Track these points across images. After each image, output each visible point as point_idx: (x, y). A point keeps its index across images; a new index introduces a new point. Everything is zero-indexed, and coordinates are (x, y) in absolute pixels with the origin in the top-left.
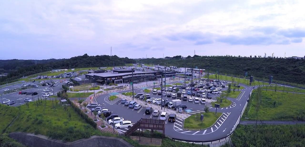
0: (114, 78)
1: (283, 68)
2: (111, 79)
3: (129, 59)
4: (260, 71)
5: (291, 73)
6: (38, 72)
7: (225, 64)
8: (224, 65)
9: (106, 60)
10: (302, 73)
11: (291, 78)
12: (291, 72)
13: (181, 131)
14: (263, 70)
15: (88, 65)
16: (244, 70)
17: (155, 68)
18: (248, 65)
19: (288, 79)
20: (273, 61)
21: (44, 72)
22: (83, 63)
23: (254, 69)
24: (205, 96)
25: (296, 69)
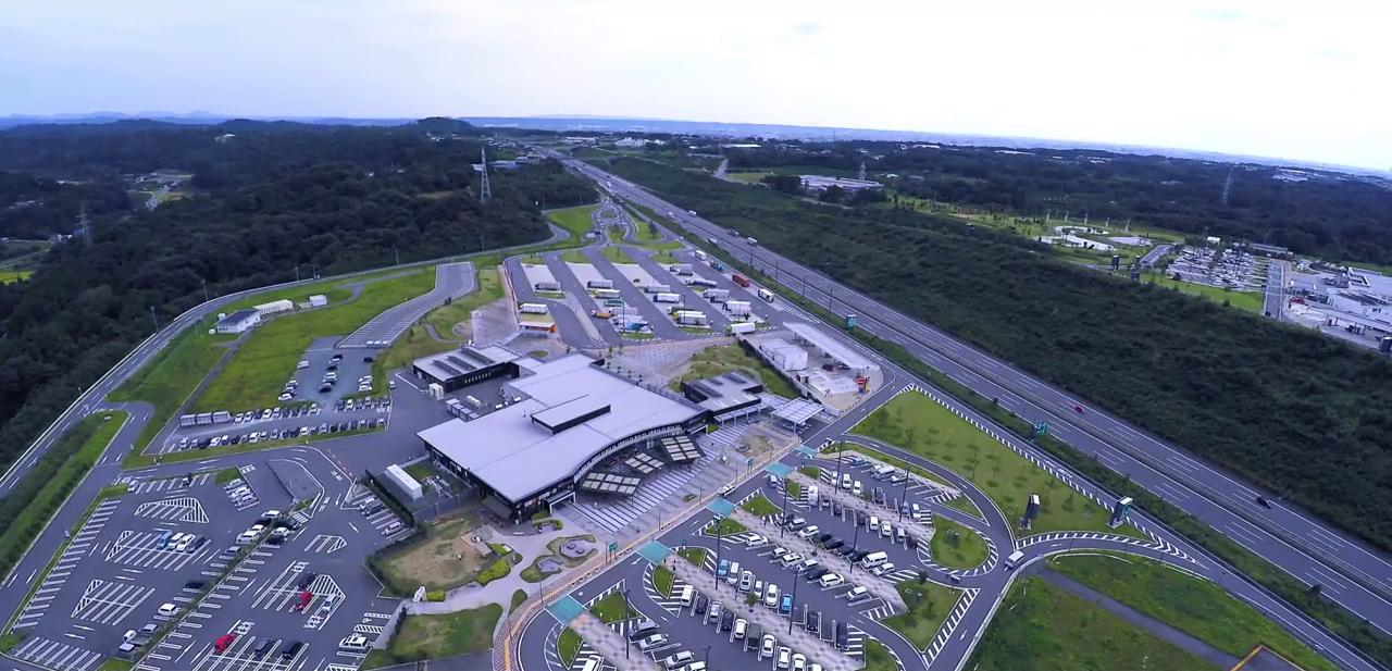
0: (548, 494)
1: (1246, 384)
2: (537, 501)
3: (592, 266)
4: (1129, 369)
5: (1276, 421)
6: (138, 333)
7: (985, 286)
8: (980, 291)
9: (464, 216)
10: (1331, 441)
11: (1264, 448)
12: (1277, 416)
13: (652, 594)
14: (1147, 365)
15: (384, 250)
16: (1060, 344)
17: (640, 215)
18: (1085, 319)
19: (1249, 452)
20: (1213, 325)
21: (170, 320)
22: (355, 242)
23: (1106, 347)
24: (859, 492)
25: (1307, 409)
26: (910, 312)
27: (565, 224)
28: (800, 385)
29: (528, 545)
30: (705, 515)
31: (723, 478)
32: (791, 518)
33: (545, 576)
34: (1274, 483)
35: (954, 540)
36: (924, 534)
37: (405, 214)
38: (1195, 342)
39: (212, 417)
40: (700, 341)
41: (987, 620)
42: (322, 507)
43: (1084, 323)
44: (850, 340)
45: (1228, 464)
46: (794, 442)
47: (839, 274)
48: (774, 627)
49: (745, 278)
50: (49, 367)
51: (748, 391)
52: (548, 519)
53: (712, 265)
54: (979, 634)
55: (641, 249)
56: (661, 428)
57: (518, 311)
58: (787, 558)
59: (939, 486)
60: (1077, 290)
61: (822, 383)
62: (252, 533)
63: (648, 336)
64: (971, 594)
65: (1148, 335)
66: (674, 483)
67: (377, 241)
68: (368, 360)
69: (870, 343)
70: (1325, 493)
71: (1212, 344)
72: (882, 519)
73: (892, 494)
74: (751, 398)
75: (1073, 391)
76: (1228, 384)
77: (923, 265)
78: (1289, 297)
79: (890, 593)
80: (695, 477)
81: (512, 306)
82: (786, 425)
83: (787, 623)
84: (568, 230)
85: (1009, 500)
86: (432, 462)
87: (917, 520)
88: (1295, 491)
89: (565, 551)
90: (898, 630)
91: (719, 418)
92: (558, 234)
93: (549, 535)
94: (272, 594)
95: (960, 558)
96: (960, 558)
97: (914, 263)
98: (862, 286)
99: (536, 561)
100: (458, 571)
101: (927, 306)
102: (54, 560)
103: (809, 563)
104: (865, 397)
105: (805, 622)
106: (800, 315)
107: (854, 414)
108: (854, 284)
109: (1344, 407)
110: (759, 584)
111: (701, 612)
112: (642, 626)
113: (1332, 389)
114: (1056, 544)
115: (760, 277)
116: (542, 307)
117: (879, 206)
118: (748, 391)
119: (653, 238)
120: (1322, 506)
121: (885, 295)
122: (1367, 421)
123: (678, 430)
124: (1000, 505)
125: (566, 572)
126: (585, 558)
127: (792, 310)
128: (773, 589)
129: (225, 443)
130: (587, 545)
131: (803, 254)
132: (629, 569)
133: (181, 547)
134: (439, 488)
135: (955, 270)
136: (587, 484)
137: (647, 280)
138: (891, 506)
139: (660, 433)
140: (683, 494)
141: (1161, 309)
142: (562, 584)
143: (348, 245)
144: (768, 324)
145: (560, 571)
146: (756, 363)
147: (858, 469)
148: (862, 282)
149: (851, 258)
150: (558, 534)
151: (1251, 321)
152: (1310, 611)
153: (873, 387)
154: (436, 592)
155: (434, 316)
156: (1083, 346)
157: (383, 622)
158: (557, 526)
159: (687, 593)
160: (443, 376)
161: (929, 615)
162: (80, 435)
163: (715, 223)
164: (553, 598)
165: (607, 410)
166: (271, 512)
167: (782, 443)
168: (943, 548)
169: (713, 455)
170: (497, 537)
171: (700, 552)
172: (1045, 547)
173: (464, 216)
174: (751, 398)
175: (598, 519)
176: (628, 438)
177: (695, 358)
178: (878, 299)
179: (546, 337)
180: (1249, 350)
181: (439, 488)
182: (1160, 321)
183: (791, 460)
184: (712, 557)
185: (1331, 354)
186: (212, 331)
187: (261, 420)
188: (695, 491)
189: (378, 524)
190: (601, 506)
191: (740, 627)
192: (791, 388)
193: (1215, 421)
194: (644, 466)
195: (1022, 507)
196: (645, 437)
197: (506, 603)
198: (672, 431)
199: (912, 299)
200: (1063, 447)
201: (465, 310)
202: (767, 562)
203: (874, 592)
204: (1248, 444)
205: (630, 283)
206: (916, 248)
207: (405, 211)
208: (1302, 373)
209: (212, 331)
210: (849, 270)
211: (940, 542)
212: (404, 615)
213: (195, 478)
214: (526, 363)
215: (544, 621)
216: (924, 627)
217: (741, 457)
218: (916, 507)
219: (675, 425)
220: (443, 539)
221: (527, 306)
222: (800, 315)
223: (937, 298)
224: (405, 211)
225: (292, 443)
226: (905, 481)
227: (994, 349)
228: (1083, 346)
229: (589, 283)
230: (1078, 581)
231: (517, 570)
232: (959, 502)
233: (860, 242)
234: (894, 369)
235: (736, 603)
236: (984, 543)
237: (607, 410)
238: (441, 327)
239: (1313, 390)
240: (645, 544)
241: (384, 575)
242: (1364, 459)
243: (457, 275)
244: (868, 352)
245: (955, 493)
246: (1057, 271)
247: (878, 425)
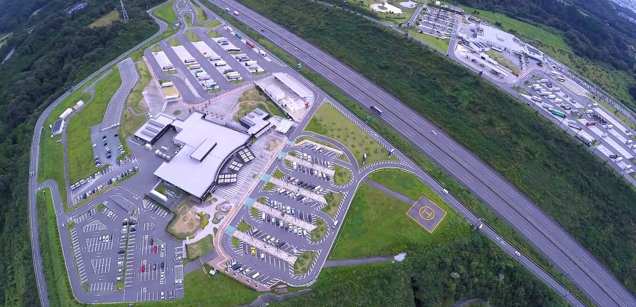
3: (182, 46)
11: (439, 112)
19: (435, 114)
22: (80, 65)
27: (163, 18)
29: (209, 210)
30: (262, 182)
31: (262, 163)
32: (289, 178)
33: (220, 220)
34: (440, 125)
35: (340, 175)
36: (331, 173)
37: (94, 39)
38: (423, 67)
39: (80, 183)
40: (239, 89)
41: (350, 202)
42: (139, 212)
43: (388, 57)
44: (300, 76)
45: (429, 118)
47: (289, 26)
48: (289, 219)
50: (9, 174)
52: (211, 198)
53: (236, 35)
54: (348, 208)
55: (202, 28)
56: (237, 149)
57: (160, 86)
58: (290, 195)
59: (335, 150)
60: (386, 40)
62: (125, 230)
64: (346, 193)
65: (409, 63)
66: (247, 171)
67: (90, 60)
68: (116, 136)
70: (454, 129)
71: (429, 68)
72: (319, 170)
73: (319, 157)
75: (383, 87)
76: (432, 86)
77: (327, 24)
78: (458, 40)
79: (322, 200)
80: (254, 166)
81: (158, 84)
83: (294, 218)
84: (167, 22)
85: (358, 152)
86: (164, 185)
87: (329, 168)
88: (446, 128)
89: (223, 210)
90: (325, 212)
91: (257, 136)
92: (163, 26)
93: (215, 204)
94: (144, 251)
95: (342, 181)
96: (342, 181)
98: (302, 35)
99: (215, 216)
100: (193, 226)
101: (329, 46)
102: (75, 257)
103: (297, 195)
104: (309, 108)
105: (299, 216)
110: (284, 207)
111: (269, 221)
112: (254, 231)
113: (463, 89)
114: (371, 168)
116: (170, 83)
119: (206, 19)
120: (453, 134)
121: (312, 40)
122: (470, 102)
123: (244, 147)
124: (355, 155)
125: (225, 217)
126: (229, 211)
127: (277, 61)
128: (288, 208)
129: (91, 194)
130: (227, 205)
131: (274, 17)
132: (243, 211)
133: (107, 241)
134: (172, 195)
135: (339, 28)
136: (220, 181)
137: (210, 53)
138: (321, 164)
139: (237, 150)
140: (252, 175)
141: (414, 51)
142: (226, 222)
143: (79, 67)
145: (223, 217)
146: (264, 98)
147: (309, 149)
148: (302, 33)
150: (217, 203)
152: (438, 180)
154: (191, 235)
155: (129, 101)
156: (387, 68)
157: (181, 249)
158: (216, 200)
159: (264, 217)
160: (149, 139)
161: (334, 205)
162: (42, 204)
164: (225, 228)
165: (216, 144)
166: (125, 220)
167: (281, 141)
168: (338, 178)
169: (257, 154)
170: (199, 210)
171: (263, 199)
172: (367, 171)
173: (120, 33)
174: (266, 123)
175: (227, 193)
177: (240, 100)
178: (309, 42)
180: (440, 72)
181: (172, 195)
182: (413, 57)
184: (267, 199)
186: (52, 136)
187: (96, 179)
188: (256, 173)
189: (160, 214)
190: (227, 187)
191: (281, 224)
193: (426, 101)
194: (236, 168)
196: (233, 153)
197: (212, 233)
198: (241, 148)
199: (323, 42)
201: (140, 92)
202: (284, 197)
203: (318, 200)
204: (435, 111)
205: (201, 54)
207: (94, 37)
208: (455, 82)
209: (52, 136)
211: (336, 176)
212: (186, 246)
213: (91, 211)
214: (176, 124)
215: (225, 236)
216: (333, 209)
217: (268, 152)
218: (329, 163)
219: (242, 146)
220: (183, 215)
221: (164, 84)
223: (333, 42)
224: (94, 37)
225: (112, 187)
226: (325, 151)
227: (356, 68)
228: (387, 68)
229: (185, 61)
230: (376, 182)
231: (210, 220)
232: (342, 157)
233: (299, 10)
235: (278, 214)
236: (350, 172)
237: (216, 144)
238: (134, 106)
240: (245, 199)
241: (174, 234)
242: (467, 116)
243: (125, 65)
244: (308, 81)
245: (341, 153)
246: (379, 31)
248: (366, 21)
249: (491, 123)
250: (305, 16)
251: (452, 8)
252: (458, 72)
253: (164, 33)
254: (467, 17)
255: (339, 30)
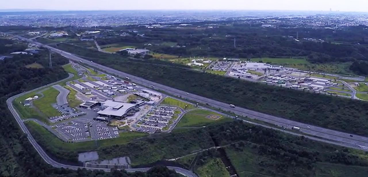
26: (164, 84)
28: (149, 99)
46: (152, 106)
49: (120, 79)
51: (142, 101)
61: (152, 98)
63: (116, 96)
65: (206, 82)
69: (158, 91)
70: (228, 100)
74: (143, 102)
77: (165, 73)
82: (149, 104)
97: (162, 73)
104: (160, 99)
106: (143, 88)
107: (159, 102)
108: (150, 79)
109: (232, 88)
115: (130, 81)
117: (151, 59)
118: (142, 101)
123: (135, 107)
144: (137, 90)
148: (152, 79)
149: (148, 73)
151: (221, 77)
153: (161, 97)
163: (111, 67)
165: (123, 106)
174: (143, 102)
176: (129, 109)
179: (96, 98)
183: (354, 88)
185: (232, 80)
192: (148, 100)
195: (185, 107)
200: (191, 101)
206: (162, 70)
209: (24, 105)
210: (148, 76)
222: (143, 88)
228: (195, 86)
233: (149, 69)
234: (164, 95)
237: (123, 106)
239: (228, 86)
247: (163, 102)
248: (185, 69)
249: (244, 94)
250: (143, 142)
251: (232, 59)
252: (230, 80)
253: (35, 24)
254: (240, 62)
255: (171, 75)
